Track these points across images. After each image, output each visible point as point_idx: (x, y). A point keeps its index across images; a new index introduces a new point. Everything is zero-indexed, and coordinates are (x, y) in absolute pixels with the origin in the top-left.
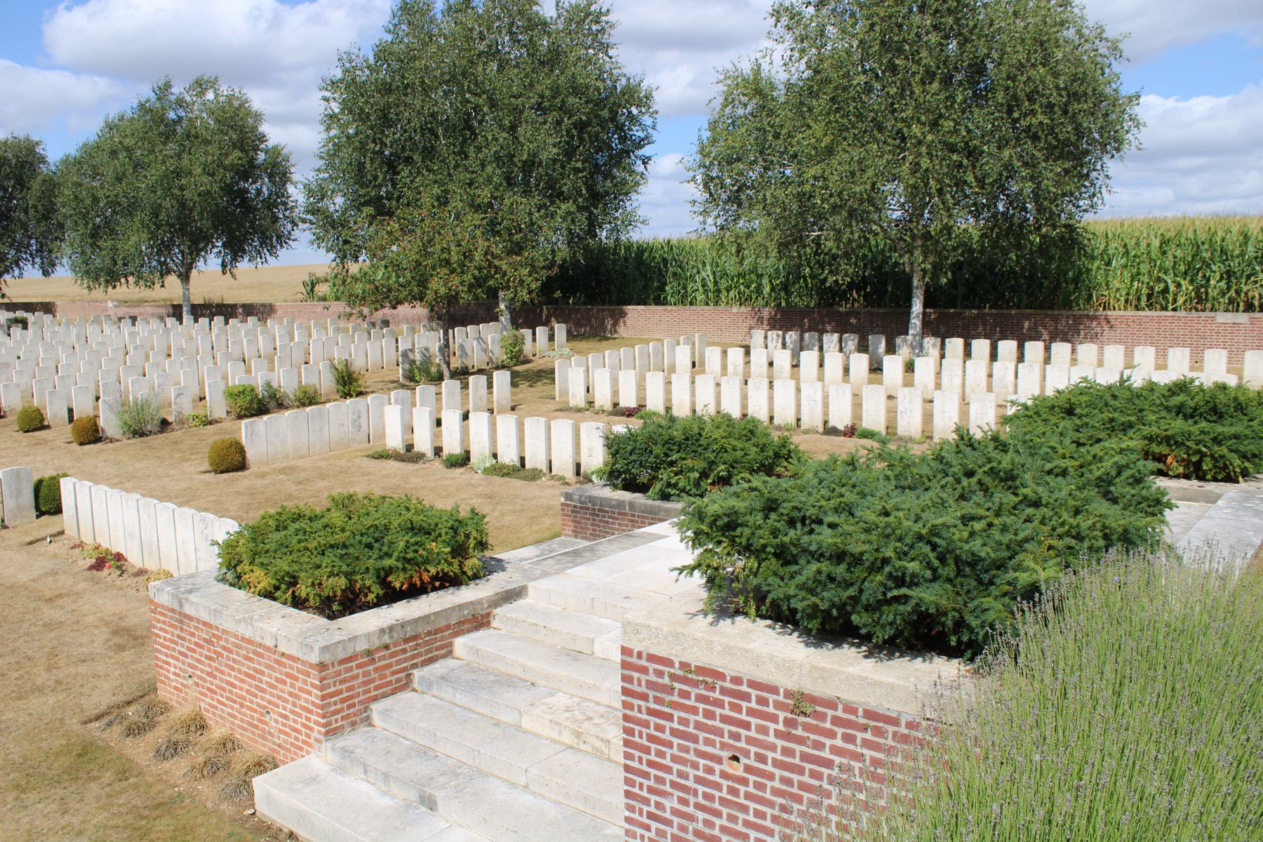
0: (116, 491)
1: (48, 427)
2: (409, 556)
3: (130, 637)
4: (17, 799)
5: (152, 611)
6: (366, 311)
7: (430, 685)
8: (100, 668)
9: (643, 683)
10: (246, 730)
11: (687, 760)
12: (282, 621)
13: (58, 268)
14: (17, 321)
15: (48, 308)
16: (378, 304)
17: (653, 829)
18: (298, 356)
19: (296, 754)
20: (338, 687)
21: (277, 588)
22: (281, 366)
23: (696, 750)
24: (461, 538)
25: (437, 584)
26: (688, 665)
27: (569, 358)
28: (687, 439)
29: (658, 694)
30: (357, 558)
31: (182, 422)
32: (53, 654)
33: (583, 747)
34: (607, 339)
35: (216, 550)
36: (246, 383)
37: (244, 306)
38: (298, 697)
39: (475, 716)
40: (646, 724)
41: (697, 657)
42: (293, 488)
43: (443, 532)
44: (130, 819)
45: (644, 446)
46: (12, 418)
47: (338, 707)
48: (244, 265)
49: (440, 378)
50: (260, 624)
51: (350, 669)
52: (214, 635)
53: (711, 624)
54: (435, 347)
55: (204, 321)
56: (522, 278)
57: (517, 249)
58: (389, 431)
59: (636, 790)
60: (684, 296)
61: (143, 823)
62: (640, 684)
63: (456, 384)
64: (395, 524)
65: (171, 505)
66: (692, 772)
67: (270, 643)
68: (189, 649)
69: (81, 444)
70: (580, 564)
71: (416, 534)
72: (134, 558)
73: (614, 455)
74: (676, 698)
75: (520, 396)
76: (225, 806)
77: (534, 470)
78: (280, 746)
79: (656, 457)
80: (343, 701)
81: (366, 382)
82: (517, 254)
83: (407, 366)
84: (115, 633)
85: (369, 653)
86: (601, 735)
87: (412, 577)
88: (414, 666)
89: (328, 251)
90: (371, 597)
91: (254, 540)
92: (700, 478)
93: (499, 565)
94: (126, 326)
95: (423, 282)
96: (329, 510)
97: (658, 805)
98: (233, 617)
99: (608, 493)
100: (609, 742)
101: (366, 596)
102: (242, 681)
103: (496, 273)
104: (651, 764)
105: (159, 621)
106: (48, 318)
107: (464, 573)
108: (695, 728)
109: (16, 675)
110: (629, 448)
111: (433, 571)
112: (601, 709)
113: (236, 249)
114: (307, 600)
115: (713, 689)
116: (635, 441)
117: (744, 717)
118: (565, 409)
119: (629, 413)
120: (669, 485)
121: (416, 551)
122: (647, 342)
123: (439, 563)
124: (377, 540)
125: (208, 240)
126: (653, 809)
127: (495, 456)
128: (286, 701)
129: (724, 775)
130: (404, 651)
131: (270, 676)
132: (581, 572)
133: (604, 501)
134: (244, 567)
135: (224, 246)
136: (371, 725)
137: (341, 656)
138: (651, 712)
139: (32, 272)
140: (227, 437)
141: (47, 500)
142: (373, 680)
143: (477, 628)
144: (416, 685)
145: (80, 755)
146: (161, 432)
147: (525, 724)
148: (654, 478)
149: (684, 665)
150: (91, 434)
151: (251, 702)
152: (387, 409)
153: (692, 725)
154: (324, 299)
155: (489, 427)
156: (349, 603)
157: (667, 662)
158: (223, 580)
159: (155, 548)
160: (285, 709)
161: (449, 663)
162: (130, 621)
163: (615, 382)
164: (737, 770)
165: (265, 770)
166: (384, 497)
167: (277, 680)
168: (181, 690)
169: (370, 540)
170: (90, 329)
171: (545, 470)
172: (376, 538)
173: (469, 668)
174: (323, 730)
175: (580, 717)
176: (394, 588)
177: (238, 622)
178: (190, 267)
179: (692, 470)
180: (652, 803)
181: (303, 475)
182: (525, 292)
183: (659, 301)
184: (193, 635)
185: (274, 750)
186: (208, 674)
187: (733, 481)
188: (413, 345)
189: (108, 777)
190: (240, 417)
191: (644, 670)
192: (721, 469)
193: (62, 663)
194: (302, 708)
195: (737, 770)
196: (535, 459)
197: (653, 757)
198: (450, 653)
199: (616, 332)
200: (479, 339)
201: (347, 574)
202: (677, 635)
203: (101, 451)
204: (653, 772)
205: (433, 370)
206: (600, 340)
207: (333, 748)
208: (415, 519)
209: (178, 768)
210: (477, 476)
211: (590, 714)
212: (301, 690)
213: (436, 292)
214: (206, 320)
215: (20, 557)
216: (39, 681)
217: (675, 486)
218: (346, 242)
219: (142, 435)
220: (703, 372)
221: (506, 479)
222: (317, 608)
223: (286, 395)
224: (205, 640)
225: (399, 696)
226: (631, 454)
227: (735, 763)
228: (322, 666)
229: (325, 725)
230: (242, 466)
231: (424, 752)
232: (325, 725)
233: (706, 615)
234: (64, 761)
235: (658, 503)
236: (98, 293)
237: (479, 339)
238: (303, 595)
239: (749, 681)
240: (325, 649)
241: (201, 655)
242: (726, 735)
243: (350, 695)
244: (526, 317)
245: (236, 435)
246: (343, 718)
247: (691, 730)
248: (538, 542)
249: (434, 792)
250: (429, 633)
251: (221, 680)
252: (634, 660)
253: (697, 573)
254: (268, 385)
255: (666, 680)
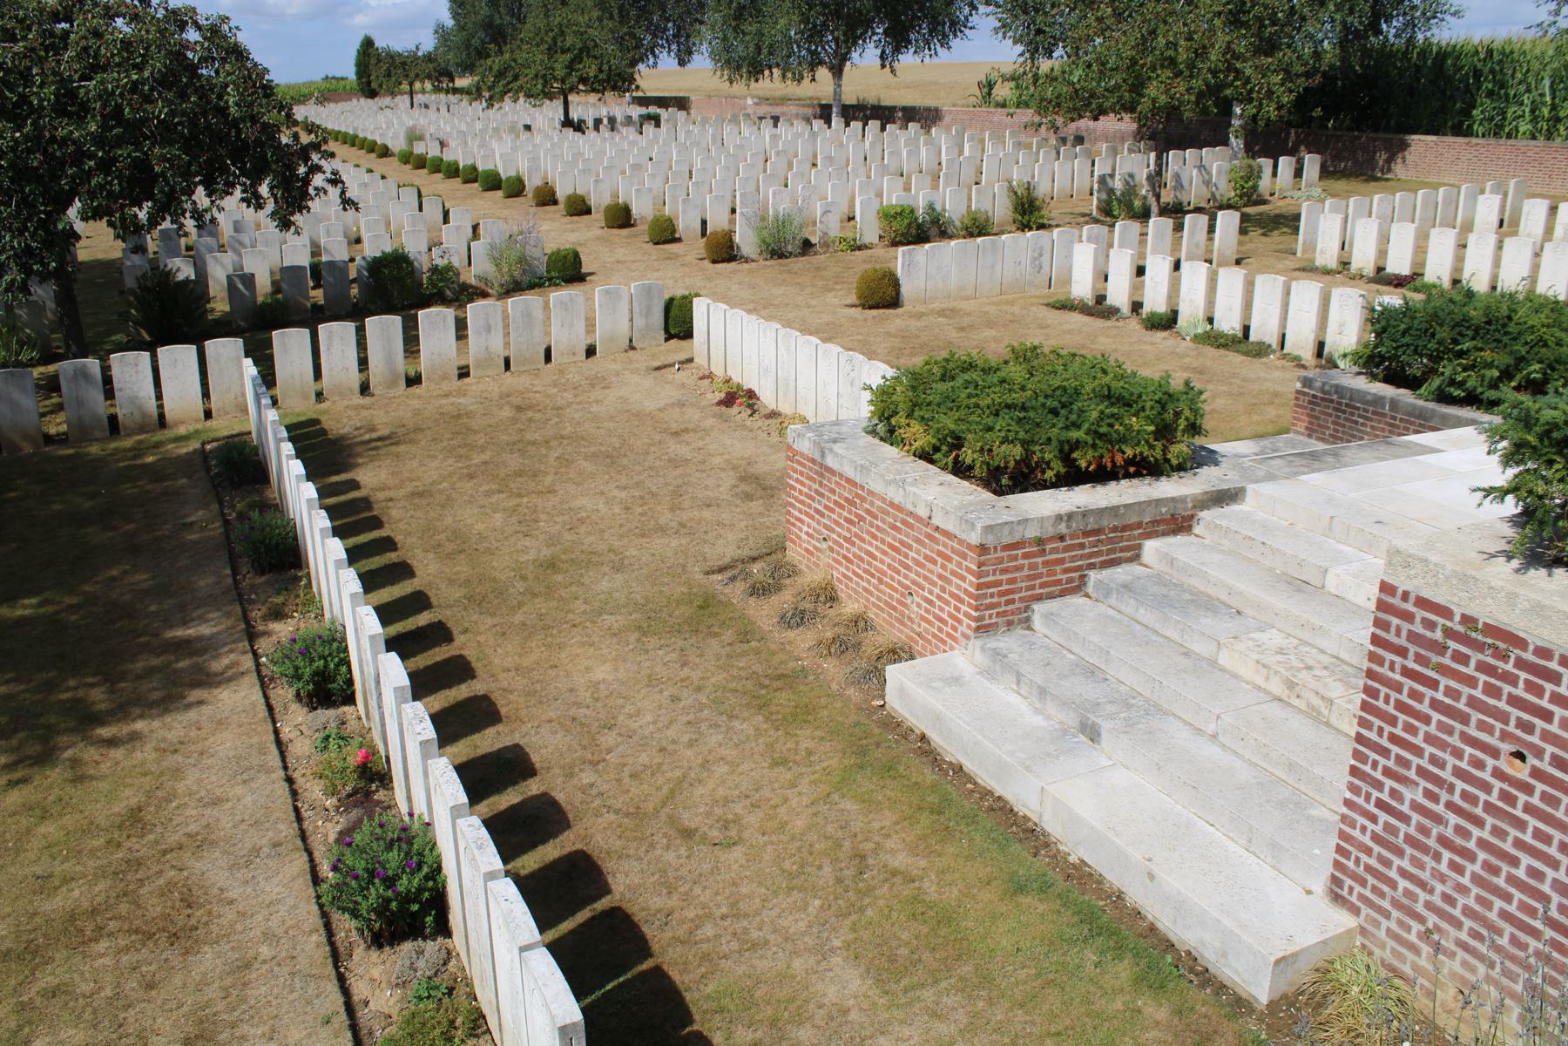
0: (754, 317)
1: (679, 240)
2: (1103, 430)
3: (759, 487)
4: (638, 640)
5: (789, 458)
6: (1060, 121)
7: (1108, 592)
8: (726, 516)
9: (1404, 633)
10: (882, 610)
11: (1448, 745)
12: (940, 489)
13: (695, 56)
14: (649, 117)
15: (682, 103)
16: (1076, 113)
17: (1381, 822)
18: (968, 174)
19: (937, 647)
20: (998, 577)
21: (936, 449)
22: (947, 184)
23: (1462, 734)
24: (1169, 416)
25: (1132, 470)
26: (1475, 621)
27: (1322, 201)
28: (1489, 323)
29: (1423, 652)
30: (1038, 425)
31: (826, 245)
32: (677, 493)
33: (1295, 702)
34: (1377, 179)
35: (867, 395)
36: (905, 203)
37: (904, 109)
38: (949, 582)
39: (1160, 640)
40: (1398, 688)
41: (1488, 611)
42: (953, 334)
43: (1148, 404)
44: (749, 685)
45: (1424, 326)
46: (643, 228)
47: (995, 600)
48: (907, 59)
49: (1144, 215)
50: (913, 489)
51: (1015, 558)
52: (857, 495)
53: (1517, 571)
54: (1142, 176)
55: (856, 125)
56: (1271, 86)
57: (1268, 47)
58: (1076, 276)
59: (1367, 769)
60: (1500, 127)
61: (763, 692)
62: (1398, 634)
63: (1168, 223)
64: (1088, 388)
65: (814, 340)
66: (1451, 761)
67: (922, 512)
68: (826, 507)
69: (714, 262)
70: (1319, 470)
71: (1112, 404)
72: (767, 398)
73: (1378, 335)
74: (1447, 661)
75: (1248, 246)
76: (851, 691)
77: (1261, 343)
78: (919, 634)
79: (1440, 343)
80: (1002, 594)
81: (1052, 212)
82: (1266, 55)
83: (1104, 196)
84: (742, 479)
85: (1040, 542)
86: (1322, 691)
87: (1102, 457)
88: (1092, 566)
89: (1015, 43)
90: (1049, 474)
91: (914, 388)
92: (1500, 379)
93: (1210, 458)
94: (767, 128)
95: (1137, 87)
96: (1006, 362)
97: (1394, 793)
98: (882, 476)
99: (1361, 383)
100: (1331, 702)
101: (1043, 472)
102: (884, 553)
103: (1236, 79)
104: (1393, 738)
105: (795, 471)
106: (681, 115)
107: (1167, 461)
108: (1468, 704)
109: (640, 510)
110: (1403, 326)
111: (1129, 452)
112: (1326, 659)
113: (898, 40)
114: (970, 468)
115: (1505, 658)
116: (1413, 318)
117: (1544, 703)
118: (1309, 269)
119: (1398, 282)
120: (1452, 382)
121: (1111, 425)
122: (1436, 187)
123: (1138, 444)
124: (1064, 406)
125: (868, 24)
126: (1385, 797)
127: (1211, 320)
128: (934, 584)
129: (1498, 774)
130: (1082, 546)
131: (918, 552)
132: (1317, 480)
133: (1355, 394)
134: (900, 419)
135: (886, 33)
136: (1029, 628)
137: (1006, 540)
138: (1407, 672)
139: (667, 61)
140: (878, 266)
141: (677, 322)
142: (1040, 576)
143: (1175, 532)
144: (1090, 590)
145: (701, 607)
146: (803, 254)
147: (1224, 659)
148: (1431, 372)
149: (1467, 620)
150: (724, 251)
151: (892, 579)
152: (1077, 247)
153: (1464, 699)
154: (1003, 105)
155: (1198, 281)
156: (1018, 478)
157: (1446, 612)
158: (873, 432)
159: (792, 384)
160: (931, 593)
161: (1135, 569)
162: (760, 468)
163: (1384, 239)
164: (1521, 772)
165: (899, 660)
166: (1074, 355)
167: (926, 557)
168: (814, 552)
169: (1056, 404)
170: (728, 129)
171: (1275, 345)
172: (1063, 402)
173: (1159, 579)
174: (974, 625)
175: (1296, 663)
176: (1079, 468)
177: (889, 483)
178: (844, 58)
179: (1490, 366)
180: (1387, 789)
181: (966, 321)
182: (1273, 106)
183: (1458, 131)
184: (833, 491)
185: (911, 639)
186: (846, 539)
187: (1550, 388)
188: (1114, 170)
189: (728, 635)
190: (895, 244)
191: (1409, 617)
192: (1535, 370)
193: (686, 505)
194: (953, 595)
195: (1521, 772)
196: (1264, 328)
197: (1398, 731)
198: (1136, 558)
199: (1389, 170)
200: (1201, 167)
201: (1024, 443)
202: (1464, 579)
203: (735, 272)
204: (1395, 749)
205: (1137, 203)
206: (1367, 181)
207: (983, 649)
208: (1114, 384)
209: (803, 640)
210: (1184, 344)
211: (1311, 663)
212: (953, 573)
213: (1154, 101)
214: (860, 124)
215: (647, 382)
216: (662, 521)
217: (1461, 385)
218: (1039, 32)
219: (782, 256)
220: (1515, 233)
221: (1222, 351)
222: (981, 479)
223: (951, 222)
224: (847, 500)
225: (1069, 599)
226: (1404, 334)
227: (1518, 762)
228: (983, 549)
229: (977, 619)
230: (894, 302)
231: (1091, 672)
232: (977, 619)
233: (1510, 558)
234: (685, 611)
235: (1431, 405)
236: (739, 87)
237: (1201, 167)
238: (968, 461)
239: (1562, 656)
240: (989, 529)
241: (840, 515)
242: (1513, 722)
243: (1011, 589)
244: (1267, 141)
245: (891, 266)
246: (998, 614)
247: (1461, 705)
248: (1259, 436)
249: (1097, 721)
250: (1115, 529)
251: (860, 549)
252: (1396, 601)
253: (1510, 499)
254: (931, 207)
255: (1438, 635)
